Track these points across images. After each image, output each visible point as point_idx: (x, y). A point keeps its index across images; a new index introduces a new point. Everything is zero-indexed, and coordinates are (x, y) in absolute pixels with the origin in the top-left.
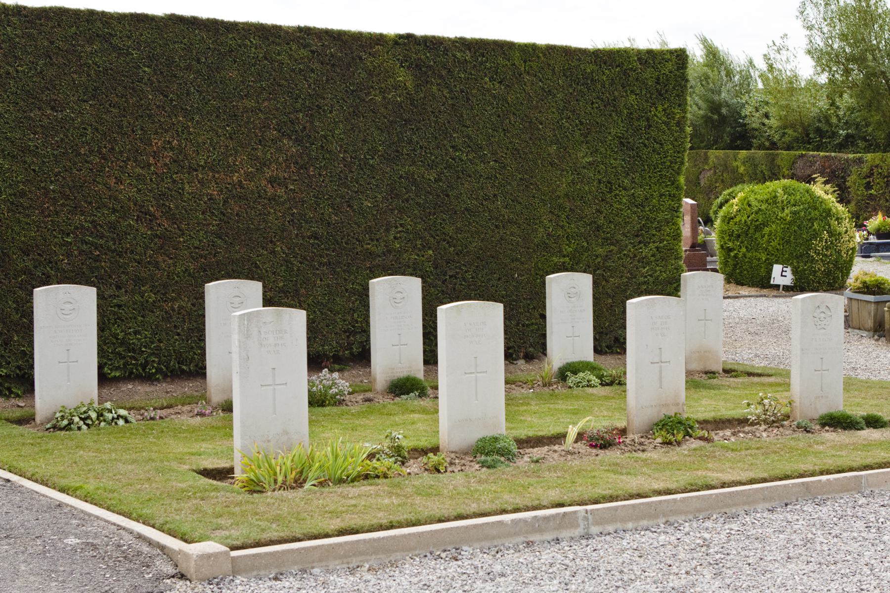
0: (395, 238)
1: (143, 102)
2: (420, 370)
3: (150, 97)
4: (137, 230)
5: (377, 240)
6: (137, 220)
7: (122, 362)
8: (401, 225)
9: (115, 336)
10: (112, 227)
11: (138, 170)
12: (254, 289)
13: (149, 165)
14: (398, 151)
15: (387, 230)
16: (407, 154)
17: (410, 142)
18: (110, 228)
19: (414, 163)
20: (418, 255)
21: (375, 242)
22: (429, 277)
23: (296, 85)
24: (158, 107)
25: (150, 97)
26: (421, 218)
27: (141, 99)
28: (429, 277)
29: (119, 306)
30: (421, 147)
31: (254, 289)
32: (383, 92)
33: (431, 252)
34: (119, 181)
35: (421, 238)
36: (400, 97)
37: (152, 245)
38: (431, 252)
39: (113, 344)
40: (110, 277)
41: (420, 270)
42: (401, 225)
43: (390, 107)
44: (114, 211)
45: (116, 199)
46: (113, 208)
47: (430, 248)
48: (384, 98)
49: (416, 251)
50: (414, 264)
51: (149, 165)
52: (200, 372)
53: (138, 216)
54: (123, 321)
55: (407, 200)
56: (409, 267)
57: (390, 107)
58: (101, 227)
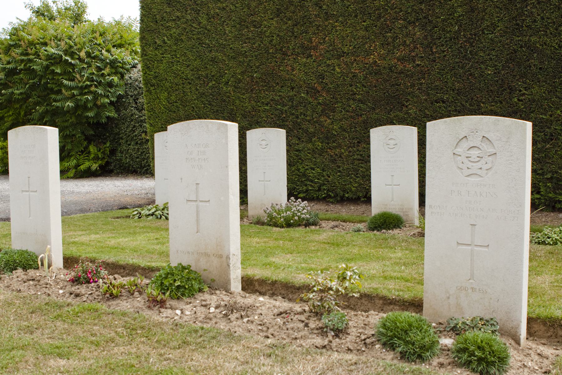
10: (291, 99)
24: (316, 16)
45: (292, 80)
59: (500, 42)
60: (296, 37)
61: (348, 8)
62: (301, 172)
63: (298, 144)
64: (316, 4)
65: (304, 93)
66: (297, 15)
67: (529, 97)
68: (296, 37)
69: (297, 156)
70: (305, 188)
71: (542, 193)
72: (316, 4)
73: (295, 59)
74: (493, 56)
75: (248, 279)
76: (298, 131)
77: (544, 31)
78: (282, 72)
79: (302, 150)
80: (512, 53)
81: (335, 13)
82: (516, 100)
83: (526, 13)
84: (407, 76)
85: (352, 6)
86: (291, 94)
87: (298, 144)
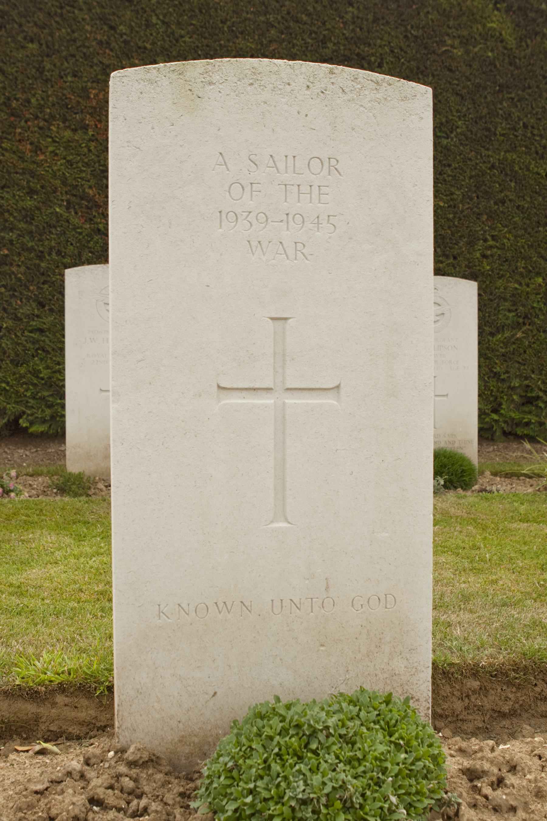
0: (484, 256)
1: (76, 35)
2: (471, 442)
3: (88, 28)
4: (68, 221)
5: (455, 258)
6: (68, 208)
7: (48, 412)
8: (493, 236)
9: (36, 373)
10: (28, 216)
11: (68, 134)
12: (78, 282)
13: (85, 128)
14: (488, 129)
15: (471, 244)
16: (503, 135)
17: (508, 116)
18: (26, 216)
19: (513, 149)
20: (520, 284)
21: (451, 260)
22: (537, 316)
23: (324, 24)
24: (100, 43)
25: (88, 28)
26: (525, 230)
27: (73, 32)
28: (537, 316)
29: (41, 331)
30: (525, 126)
31: (78, 282)
32: (465, 42)
33: (540, 280)
34: (37, 149)
35: (524, 258)
36: (492, 51)
37: (91, 244)
38: (540, 280)
39: (35, 385)
40: (27, 288)
41: (523, 306)
42: (493, 236)
43: (476, 65)
44: (31, 192)
45: (33, 174)
46: (29, 187)
47: (538, 274)
48: (467, 52)
49: (517, 277)
50: (513, 295)
51: (85, 128)
52: (58, 435)
53: (68, 202)
54: (48, 352)
55: (503, 202)
56: (505, 300)
57: (476, 65)
58: (11, 214)
59: (461, 154)
60: (47, 81)
61: (177, 41)
62: (42, 379)
63: (38, 316)
64: (103, 19)
65: (60, 206)
66: (52, 34)
67: (499, 252)
68: (47, 81)
69: (33, 343)
70: (48, 412)
71: (502, 411)
72: (101, 19)
73: (41, 128)
74: (449, 176)
75: (461, 458)
76: (38, 288)
77: (526, 147)
78: (7, 154)
79: (49, 329)
80: (478, 175)
81: (148, 46)
82: (478, 255)
83: (501, 112)
84: (54, 141)
85: (187, 39)
86: (29, 203)
87: (38, 316)
